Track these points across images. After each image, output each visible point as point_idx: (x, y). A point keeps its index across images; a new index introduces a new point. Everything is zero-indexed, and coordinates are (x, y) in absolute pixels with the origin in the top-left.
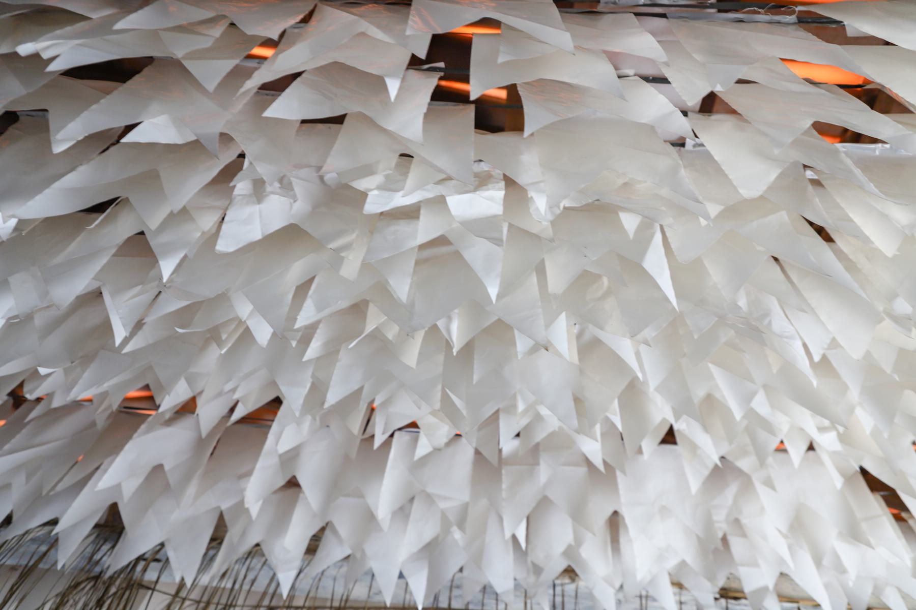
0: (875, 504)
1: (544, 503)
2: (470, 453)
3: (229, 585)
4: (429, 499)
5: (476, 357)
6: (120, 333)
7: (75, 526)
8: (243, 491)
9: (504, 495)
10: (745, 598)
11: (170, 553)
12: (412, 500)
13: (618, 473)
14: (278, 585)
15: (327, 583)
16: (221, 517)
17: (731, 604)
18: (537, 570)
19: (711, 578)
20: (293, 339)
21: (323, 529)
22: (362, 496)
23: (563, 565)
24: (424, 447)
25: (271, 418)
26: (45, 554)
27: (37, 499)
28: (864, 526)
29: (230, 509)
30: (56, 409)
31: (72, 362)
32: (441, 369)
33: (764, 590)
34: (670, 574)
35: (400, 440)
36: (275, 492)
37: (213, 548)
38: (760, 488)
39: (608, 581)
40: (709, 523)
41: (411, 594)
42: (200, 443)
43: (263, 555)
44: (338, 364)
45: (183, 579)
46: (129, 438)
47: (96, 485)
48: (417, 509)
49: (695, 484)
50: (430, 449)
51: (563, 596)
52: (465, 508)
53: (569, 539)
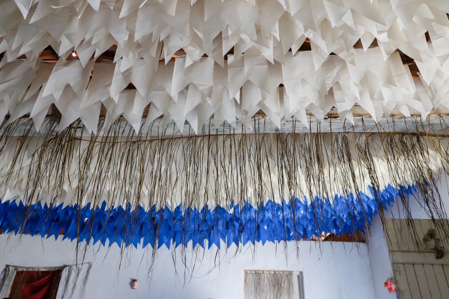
0: (405, 69)
1: (248, 83)
2: (213, 63)
3: (113, 135)
4: (195, 87)
5: (205, 8)
6: (25, 13)
7: (38, 114)
8: (109, 93)
9: (229, 81)
10: (339, 117)
11: (84, 122)
12: (187, 88)
13: (282, 66)
14: (134, 131)
15: (155, 129)
16: (103, 106)
17: (332, 120)
18: (246, 113)
19: (323, 109)
20: (111, 6)
21: (149, 106)
22: (164, 90)
23: (257, 110)
24: (189, 62)
25: (145, 113)
26: (30, 129)
27: (18, 105)
28: (395, 79)
29: (105, 101)
30: (10, 63)
31: (7, 32)
32: (188, 17)
33: (346, 112)
34: (306, 110)
35: (178, 61)
36: (123, 92)
37: (102, 120)
38: (349, 66)
39: (277, 114)
40: (323, 85)
41: (192, 130)
42: (84, 71)
43: (125, 120)
44: (138, 20)
45: (93, 132)
46: (50, 73)
47: (41, 95)
48: (190, 92)
49: (317, 66)
50: (191, 63)
51: (259, 124)
52: (211, 88)
53: (260, 99)
